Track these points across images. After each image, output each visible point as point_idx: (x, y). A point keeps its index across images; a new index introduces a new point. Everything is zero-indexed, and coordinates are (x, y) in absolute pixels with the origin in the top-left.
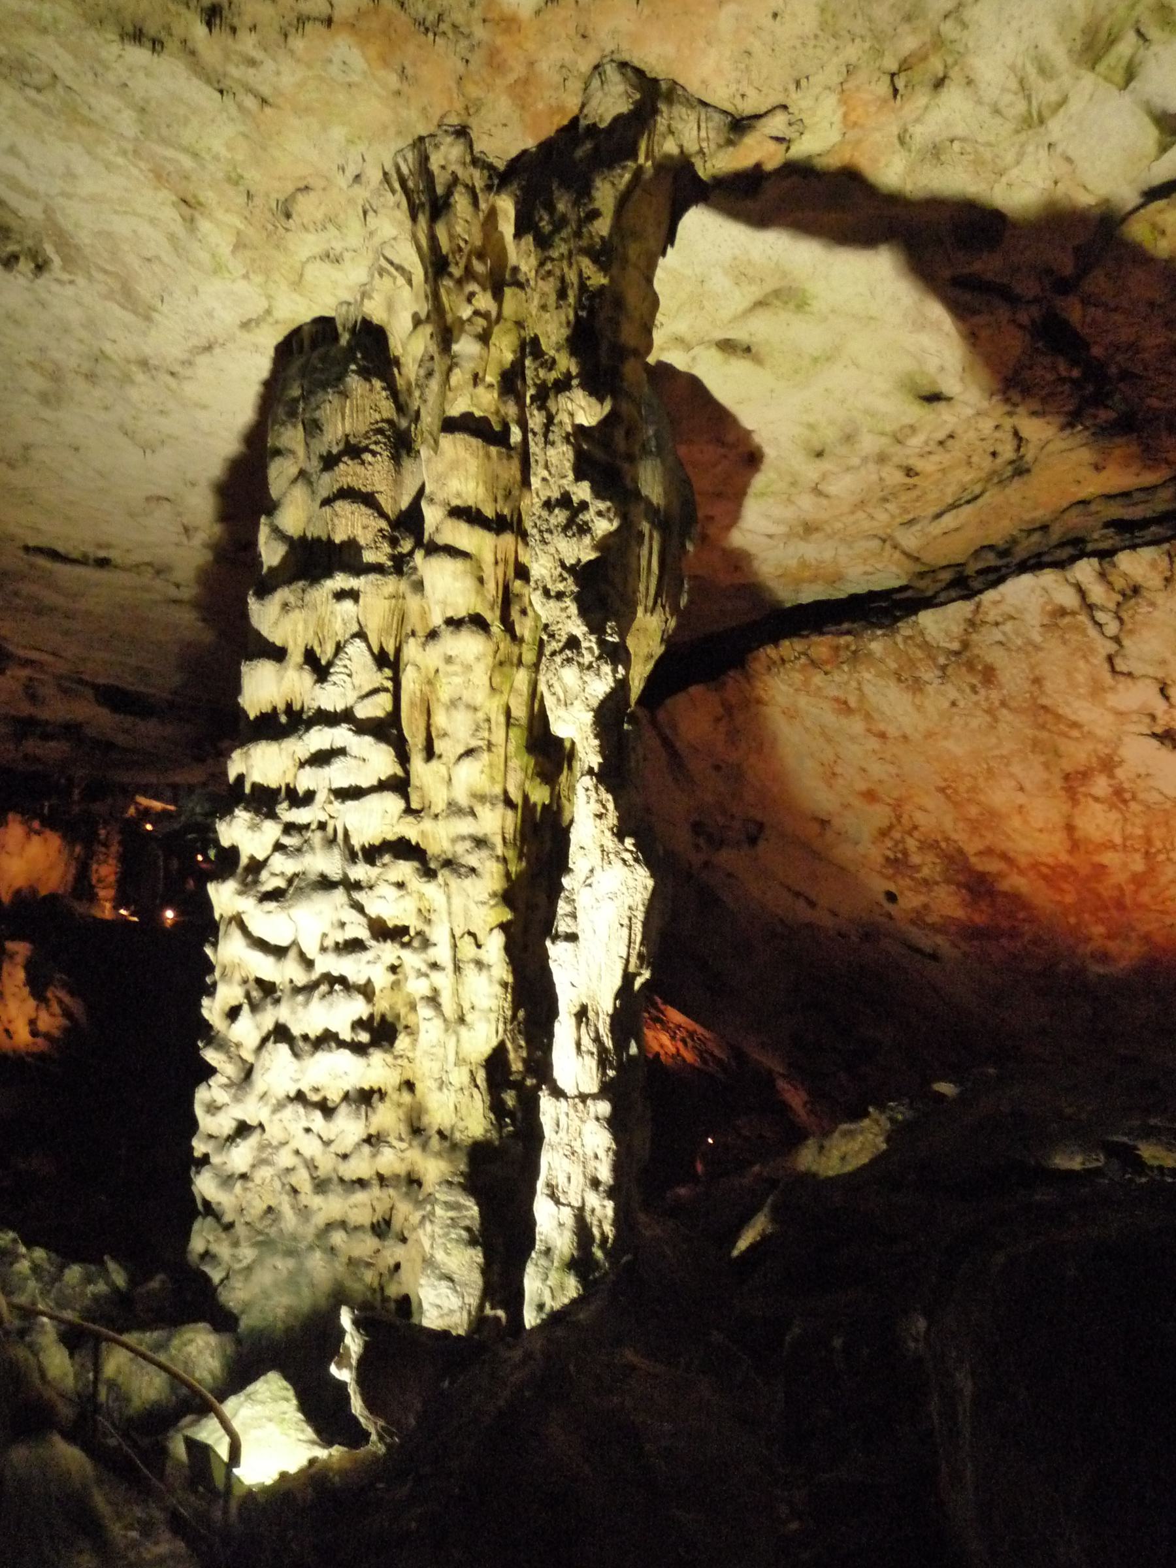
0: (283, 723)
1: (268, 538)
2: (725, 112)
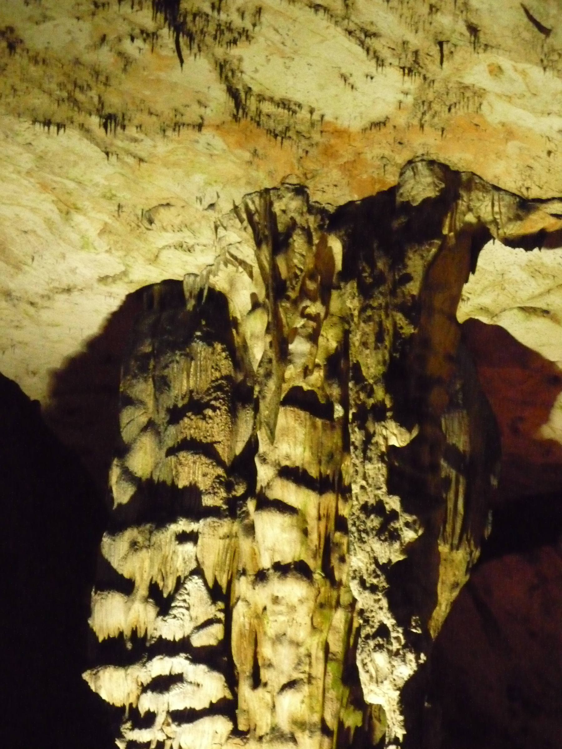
0: (130, 650)
1: (119, 478)
2: (513, 195)
